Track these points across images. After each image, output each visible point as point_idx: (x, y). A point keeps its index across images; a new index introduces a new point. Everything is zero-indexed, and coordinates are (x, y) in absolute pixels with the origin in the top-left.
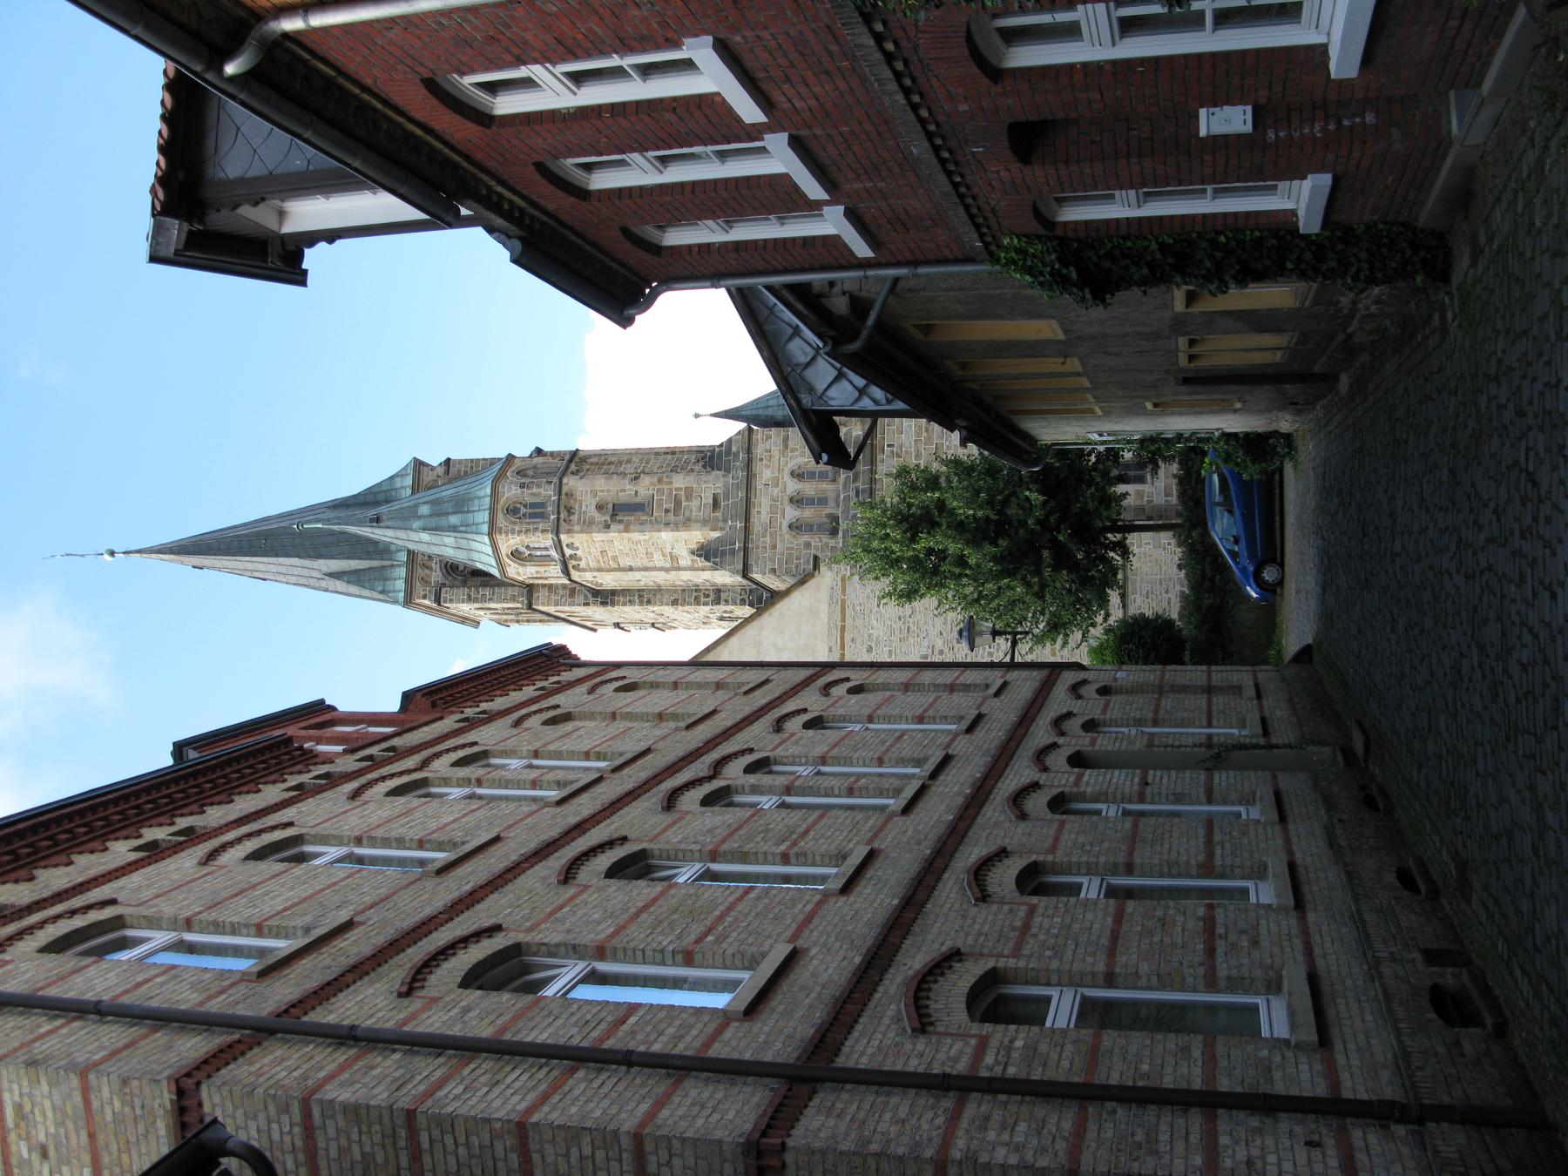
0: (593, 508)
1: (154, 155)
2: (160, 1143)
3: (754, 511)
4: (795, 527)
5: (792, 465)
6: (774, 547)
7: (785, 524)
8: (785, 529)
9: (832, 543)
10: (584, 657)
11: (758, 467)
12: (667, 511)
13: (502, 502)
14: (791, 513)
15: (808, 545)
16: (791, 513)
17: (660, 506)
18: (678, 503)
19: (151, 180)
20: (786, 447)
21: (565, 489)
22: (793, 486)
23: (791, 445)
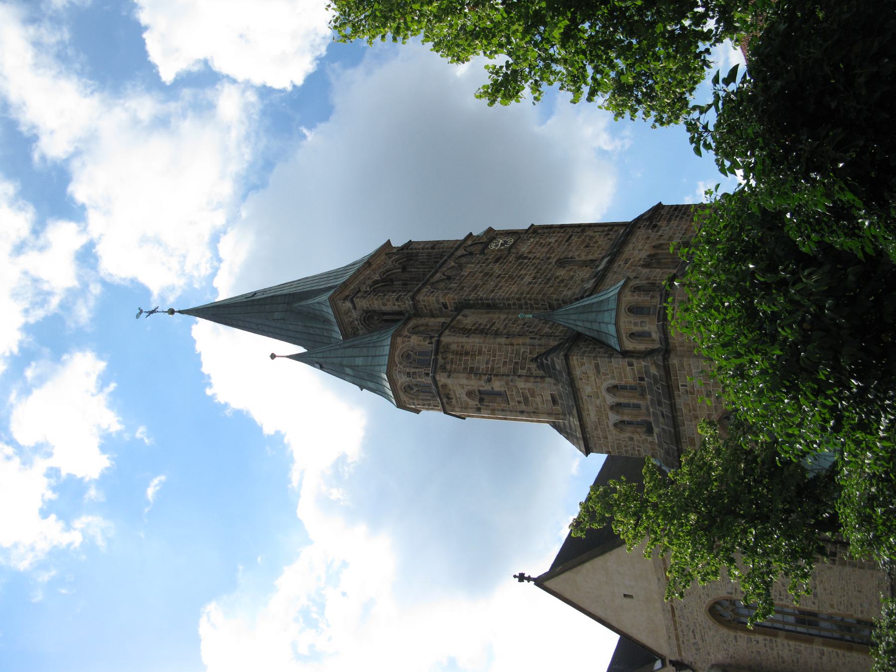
0: (465, 396)
1: (236, 404)
2: (6, 545)
3: (585, 414)
4: (618, 425)
5: (606, 384)
6: (606, 438)
7: (611, 424)
8: (611, 428)
9: (650, 439)
10: (629, 218)
11: (579, 384)
12: (519, 402)
13: (399, 384)
14: (614, 417)
15: (632, 439)
16: (614, 417)
17: (513, 399)
18: (526, 399)
19: (203, 358)
20: (598, 371)
21: (440, 384)
22: (610, 400)
23: (602, 370)
